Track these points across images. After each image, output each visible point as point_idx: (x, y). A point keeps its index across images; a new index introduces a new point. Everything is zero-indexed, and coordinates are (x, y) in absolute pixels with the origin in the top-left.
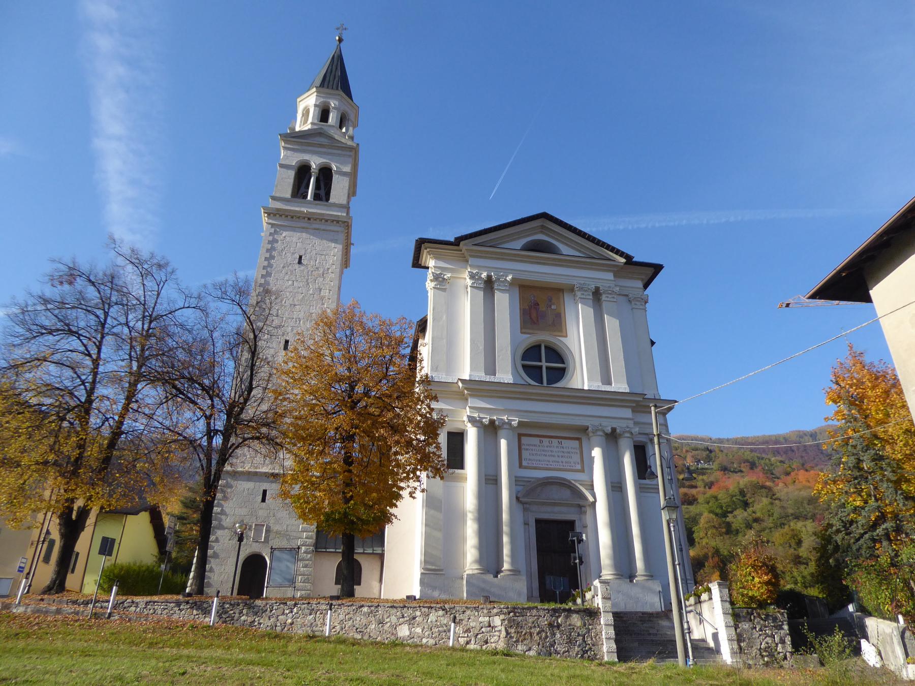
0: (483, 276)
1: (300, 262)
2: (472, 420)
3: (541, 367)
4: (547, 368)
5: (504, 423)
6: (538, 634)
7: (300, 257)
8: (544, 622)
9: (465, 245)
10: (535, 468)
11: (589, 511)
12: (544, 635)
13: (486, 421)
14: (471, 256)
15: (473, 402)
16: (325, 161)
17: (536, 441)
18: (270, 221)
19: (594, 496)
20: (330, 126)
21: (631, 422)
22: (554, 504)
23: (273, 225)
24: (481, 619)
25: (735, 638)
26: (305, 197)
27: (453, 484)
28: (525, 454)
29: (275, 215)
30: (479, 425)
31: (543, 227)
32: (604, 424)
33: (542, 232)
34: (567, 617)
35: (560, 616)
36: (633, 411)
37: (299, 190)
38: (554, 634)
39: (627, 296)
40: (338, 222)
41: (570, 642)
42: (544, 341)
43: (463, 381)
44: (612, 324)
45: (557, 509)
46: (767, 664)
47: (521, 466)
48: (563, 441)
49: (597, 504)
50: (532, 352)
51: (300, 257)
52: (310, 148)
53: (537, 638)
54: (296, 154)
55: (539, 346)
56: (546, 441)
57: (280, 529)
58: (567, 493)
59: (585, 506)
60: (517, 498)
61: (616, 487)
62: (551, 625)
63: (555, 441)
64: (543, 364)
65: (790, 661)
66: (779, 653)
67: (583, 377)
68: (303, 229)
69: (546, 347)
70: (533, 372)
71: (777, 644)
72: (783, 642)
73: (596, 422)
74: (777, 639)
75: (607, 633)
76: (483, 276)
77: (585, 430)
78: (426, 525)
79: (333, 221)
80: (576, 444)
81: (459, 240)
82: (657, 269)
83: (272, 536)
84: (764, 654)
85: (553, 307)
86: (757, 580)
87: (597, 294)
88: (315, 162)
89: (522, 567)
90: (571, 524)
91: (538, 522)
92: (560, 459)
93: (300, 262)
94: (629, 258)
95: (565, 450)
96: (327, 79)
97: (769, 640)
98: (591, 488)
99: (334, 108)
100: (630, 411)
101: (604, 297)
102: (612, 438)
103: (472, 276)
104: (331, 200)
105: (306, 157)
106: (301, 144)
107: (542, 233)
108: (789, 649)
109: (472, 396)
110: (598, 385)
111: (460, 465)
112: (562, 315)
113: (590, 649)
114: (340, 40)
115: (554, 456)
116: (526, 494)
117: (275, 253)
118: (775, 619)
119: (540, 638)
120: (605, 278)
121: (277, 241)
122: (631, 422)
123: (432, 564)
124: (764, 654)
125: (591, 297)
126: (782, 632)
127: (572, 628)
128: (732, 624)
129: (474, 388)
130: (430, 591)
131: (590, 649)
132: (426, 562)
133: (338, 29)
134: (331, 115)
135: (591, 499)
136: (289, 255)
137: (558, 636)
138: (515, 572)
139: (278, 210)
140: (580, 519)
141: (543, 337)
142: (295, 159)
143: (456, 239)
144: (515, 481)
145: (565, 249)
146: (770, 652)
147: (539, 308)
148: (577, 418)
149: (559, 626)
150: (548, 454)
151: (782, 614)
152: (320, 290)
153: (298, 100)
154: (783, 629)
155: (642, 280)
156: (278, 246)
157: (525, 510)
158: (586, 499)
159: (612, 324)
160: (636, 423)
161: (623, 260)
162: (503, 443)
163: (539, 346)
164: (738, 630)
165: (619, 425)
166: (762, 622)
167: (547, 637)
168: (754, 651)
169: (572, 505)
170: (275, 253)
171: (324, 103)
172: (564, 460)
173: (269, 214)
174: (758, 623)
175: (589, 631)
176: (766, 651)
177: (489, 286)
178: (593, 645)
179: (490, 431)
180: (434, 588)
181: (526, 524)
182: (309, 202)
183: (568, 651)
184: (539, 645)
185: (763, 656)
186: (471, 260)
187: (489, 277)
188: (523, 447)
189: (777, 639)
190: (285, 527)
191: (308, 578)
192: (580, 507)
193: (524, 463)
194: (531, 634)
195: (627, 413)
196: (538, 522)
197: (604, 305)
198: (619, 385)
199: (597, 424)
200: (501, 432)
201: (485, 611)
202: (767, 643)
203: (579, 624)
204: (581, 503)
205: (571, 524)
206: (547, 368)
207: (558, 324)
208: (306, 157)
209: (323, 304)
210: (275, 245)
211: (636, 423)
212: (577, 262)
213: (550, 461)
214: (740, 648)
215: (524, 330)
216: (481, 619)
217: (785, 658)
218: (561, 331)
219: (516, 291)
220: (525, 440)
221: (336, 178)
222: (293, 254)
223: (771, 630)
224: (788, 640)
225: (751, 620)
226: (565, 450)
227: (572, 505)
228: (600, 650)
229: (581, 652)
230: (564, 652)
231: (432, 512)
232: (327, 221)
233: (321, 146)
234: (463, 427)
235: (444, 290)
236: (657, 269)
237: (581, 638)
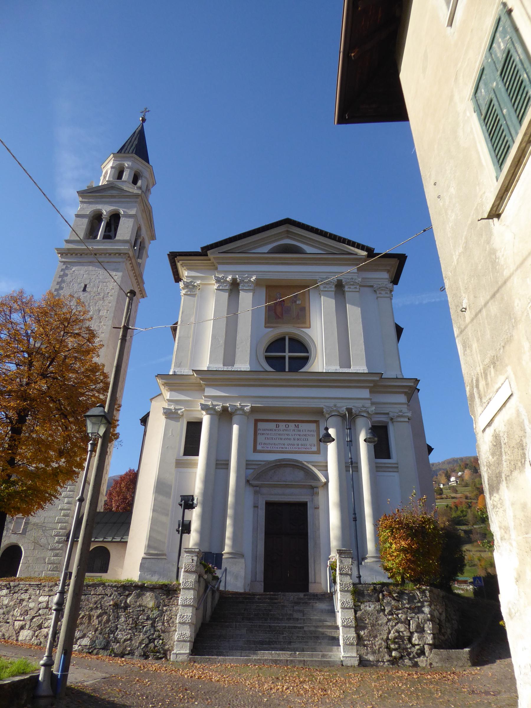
0: (228, 279)
1: (84, 290)
2: (204, 407)
3: (284, 358)
4: (290, 358)
5: (237, 409)
6: (98, 617)
7: (86, 286)
8: (109, 602)
9: (212, 254)
10: (270, 452)
11: (321, 491)
12: (105, 618)
13: (218, 408)
14: (219, 263)
15: (210, 392)
16: (114, 208)
17: (273, 425)
18: (63, 260)
19: (327, 477)
20: (123, 181)
21: (369, 402)
22: (286, 486)
23: (64, 263)
24: (41, 599)
25: (353, 624)
26: (96, 237)
27: (185, 470)
28: (260, 439)
29: (67, 255)
30: (212, 412)
31: (288, 232)
32: (339, 405)
33: (288, 237)
34: (139, 596)
35: (129, 595)
36: (371, 392)
37: (92, 232)
38: (118, 617)
39: (372, 286)
40: (120, 254)
41: (136, 626)
42: (288, 333)
43: (197, 372)
44: (354, 313)
45: (288, 491)
46: (394, 662)
47: (255, 450)
48: (300, 424)
49: (329, 484)
50: (277, 344)
51: (86, 286)
52: (104, 200)
53: (95, 622)
54: (91, 206)
55: (283, 339)
56: (282, 425)
57: (37, 521)
58: (301, 474)
59: (316, 487)
60: (248, 481)
61: (349, 466)
62: (116, 606)
63: (292, 425)
64: (286, 354)
65: (432, 657)
66: (414, 645)
67: (321, 362)
68: (91, 263)
69: (290, 339)
70: (276, 363)
71: (412, 633)
72: (421, 630)
73: (331, 403)
74: (413, 626)
75: (182, 617)
76: (228, 279)
77: (320, 412)
78: (154, 510)
79: (115, 254)
80: (313, 426)
81: (205, 251)
82: (401, 259)
83: (30, 527)
84: (392, 646)
85: (298, 302)
86: (394, 546)
87: (340, 286)
88: (106, 210)
89: (248, 550)
90: (303, 506)
91: (268, 504)
92: (296, 442)
93: (84, 290)
94: (371, 253)
95: (301, 433)
96: (125, 148)
97: (401, 627)
98: (325, 469)
99: (128, 168)
100: (368, 391)
101: (346, 289)
102: (348, 420)
103: (218, 280)
104: (117, 238)
105: (99, 207)
106: (96, 197)
107: (286, 236)
108: (429, 639)
109: (208, 386)
110: (335, 368)
111: (196, 453)
112: (307, 308)
113: (159, 636)
114: (144, 120)
115: (290, 439)
116: (256, 476)
117: (64, 285)
118: (412, 599)
119: (100, 622)
120: (346, 272)
121: (67, 275)
122: (369, 402)
123: (155, 548)
124: (392, 646)
125: (333, 289)
126: (421, 616)
127: (143, 609)
128: (351, 604)
129: (210, 378)
130: (149, 577)
131: (159, 636)
132: (149, 546)
133: (142, 112)
134: (125, 173)
135: (323, 480)
136: (76, 285)
137: (122, 619)
138: (236, 555)
139: (68, 249)
140: (312, 500)
141: (286, 329)
142: (89, 209)
143: (203, 248)
144: (246, 464)
145: (308, 249)
146: (401, 643)
147: (284, 305)
148: (312, 400)
149: (126, 607)
150: (283, 437)
151: (423, 592)
152: (99, 311)
153: (102, 167)
154: (423, 612)
155: (388, 271)
156: (68, 279)
157: (256, 493)
158: (315, 478)
159: (354, 313)
160: (373, 404)
161: (365, 253)
162: (235, 428)
163: (283, 339)
164: (359, 613)
165: (356, 406)
166: (393, 602)
167: (108, 621)
168: (378, 642)
169: (303, 487)
170: (64, 285)
171: (120, 164)
172: (300, 442)
173: (62, 254)
174: (389, 603)
175: (162, 613)
176: (395, 643)
177: (234, 288)
178: (164, 632)
179: (223, 417)
180: (154, 573)
181: (256, 507)
182: (99, 242)
183: (130, 639)
184: (96, 630)
185: (390, 650)
186: (220, 267)
187: (234, 280)
188: (259, 432)
189: (413, 626)
190: (42, 519)
191: (57, 567)
192: (312, 488)
193: (259, 447)
194: (90, 617)
195: (365, 393)
196: (268, 504)
197: (347, 295)
198: (359, 366)
199: (332, 405)
200: (235, 418)
201: (47, 589)
202: (398, 632)
203: (151, 604)
204: (313, 484)
205: (303, 506)
206: (290, 358)
207: (302, 316)
208: (99, 207)
209: (100, 322)
210: (65, 278)
211: (373, 404)
212: (320, 259)
213: (284, 443)
214: (359, 638)
215: (268, 325)
216: (41, 599)
217: (422, 652)
218: (304, 323)
219: (262, 293)
220: (261, 425)
221: (122, 220)
222: (80, 283)
223: (406, 613)
224: (428, 627)
225: (378, 600)
226: (301, 433)
227: (303, 487)
228: (170, 638)
229: (146, 641)
230: (125, 640)
231: (161, 498)
232: (110, 254)
233: (113, 197)
234: (199, 416)
235: (194, 296)
236: (401, 259)
237: (150, 622)
